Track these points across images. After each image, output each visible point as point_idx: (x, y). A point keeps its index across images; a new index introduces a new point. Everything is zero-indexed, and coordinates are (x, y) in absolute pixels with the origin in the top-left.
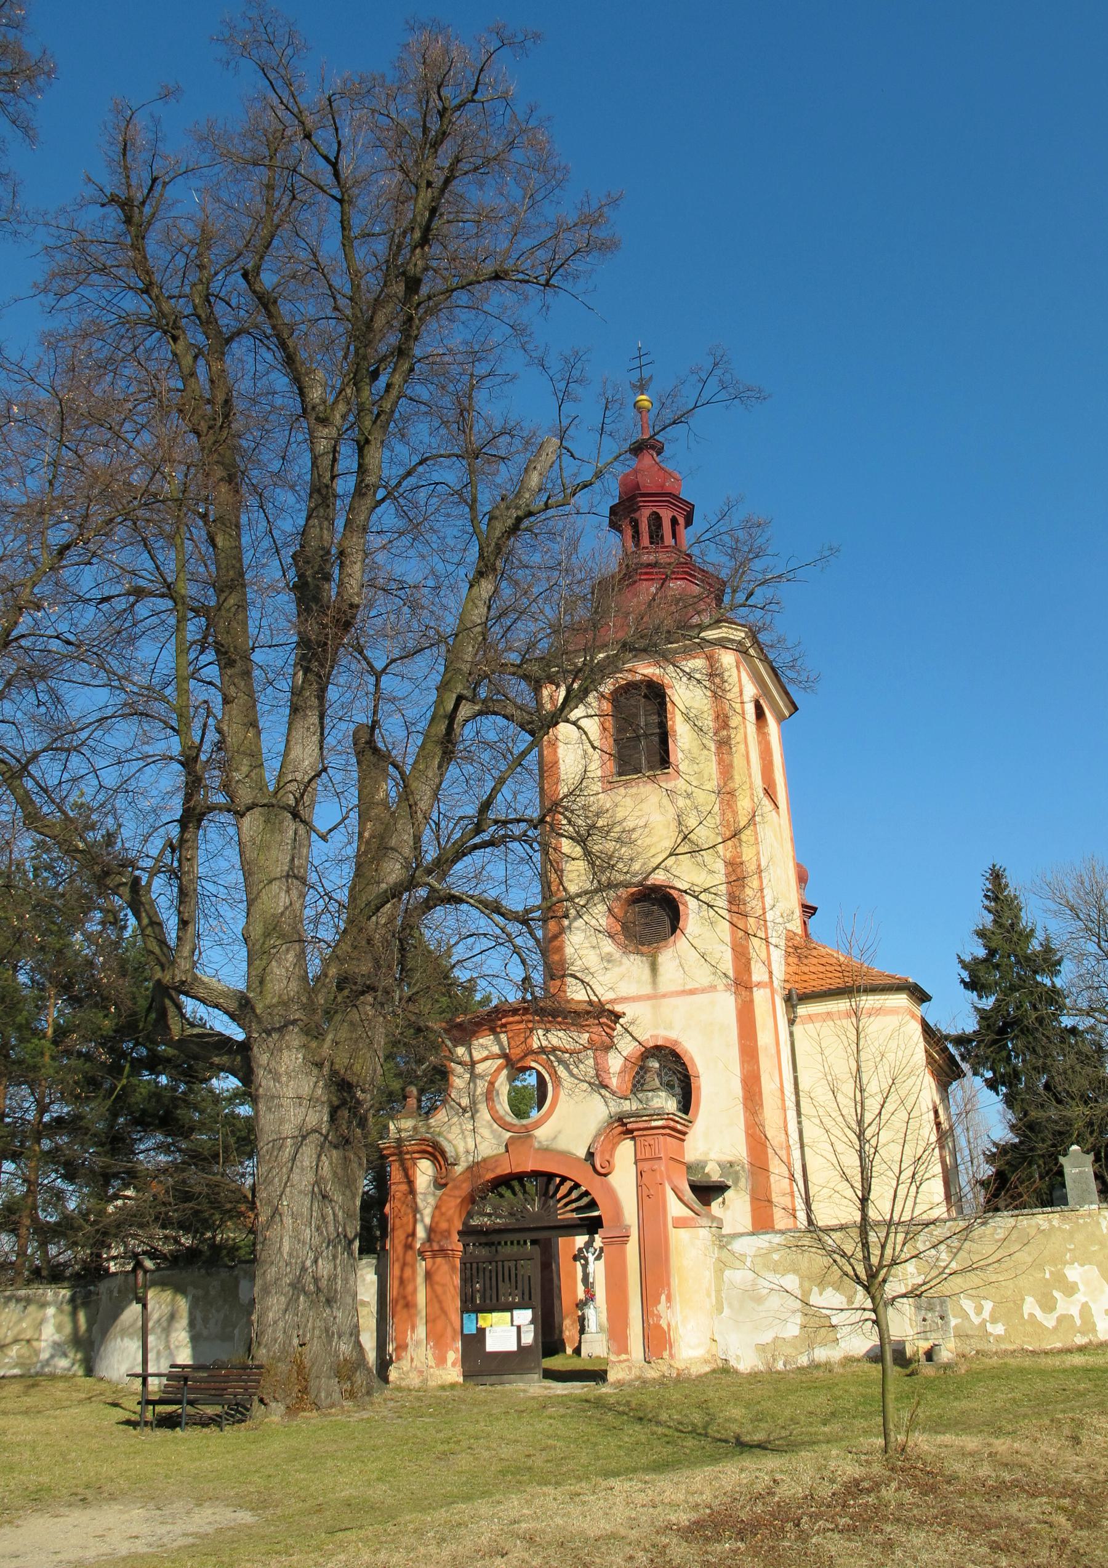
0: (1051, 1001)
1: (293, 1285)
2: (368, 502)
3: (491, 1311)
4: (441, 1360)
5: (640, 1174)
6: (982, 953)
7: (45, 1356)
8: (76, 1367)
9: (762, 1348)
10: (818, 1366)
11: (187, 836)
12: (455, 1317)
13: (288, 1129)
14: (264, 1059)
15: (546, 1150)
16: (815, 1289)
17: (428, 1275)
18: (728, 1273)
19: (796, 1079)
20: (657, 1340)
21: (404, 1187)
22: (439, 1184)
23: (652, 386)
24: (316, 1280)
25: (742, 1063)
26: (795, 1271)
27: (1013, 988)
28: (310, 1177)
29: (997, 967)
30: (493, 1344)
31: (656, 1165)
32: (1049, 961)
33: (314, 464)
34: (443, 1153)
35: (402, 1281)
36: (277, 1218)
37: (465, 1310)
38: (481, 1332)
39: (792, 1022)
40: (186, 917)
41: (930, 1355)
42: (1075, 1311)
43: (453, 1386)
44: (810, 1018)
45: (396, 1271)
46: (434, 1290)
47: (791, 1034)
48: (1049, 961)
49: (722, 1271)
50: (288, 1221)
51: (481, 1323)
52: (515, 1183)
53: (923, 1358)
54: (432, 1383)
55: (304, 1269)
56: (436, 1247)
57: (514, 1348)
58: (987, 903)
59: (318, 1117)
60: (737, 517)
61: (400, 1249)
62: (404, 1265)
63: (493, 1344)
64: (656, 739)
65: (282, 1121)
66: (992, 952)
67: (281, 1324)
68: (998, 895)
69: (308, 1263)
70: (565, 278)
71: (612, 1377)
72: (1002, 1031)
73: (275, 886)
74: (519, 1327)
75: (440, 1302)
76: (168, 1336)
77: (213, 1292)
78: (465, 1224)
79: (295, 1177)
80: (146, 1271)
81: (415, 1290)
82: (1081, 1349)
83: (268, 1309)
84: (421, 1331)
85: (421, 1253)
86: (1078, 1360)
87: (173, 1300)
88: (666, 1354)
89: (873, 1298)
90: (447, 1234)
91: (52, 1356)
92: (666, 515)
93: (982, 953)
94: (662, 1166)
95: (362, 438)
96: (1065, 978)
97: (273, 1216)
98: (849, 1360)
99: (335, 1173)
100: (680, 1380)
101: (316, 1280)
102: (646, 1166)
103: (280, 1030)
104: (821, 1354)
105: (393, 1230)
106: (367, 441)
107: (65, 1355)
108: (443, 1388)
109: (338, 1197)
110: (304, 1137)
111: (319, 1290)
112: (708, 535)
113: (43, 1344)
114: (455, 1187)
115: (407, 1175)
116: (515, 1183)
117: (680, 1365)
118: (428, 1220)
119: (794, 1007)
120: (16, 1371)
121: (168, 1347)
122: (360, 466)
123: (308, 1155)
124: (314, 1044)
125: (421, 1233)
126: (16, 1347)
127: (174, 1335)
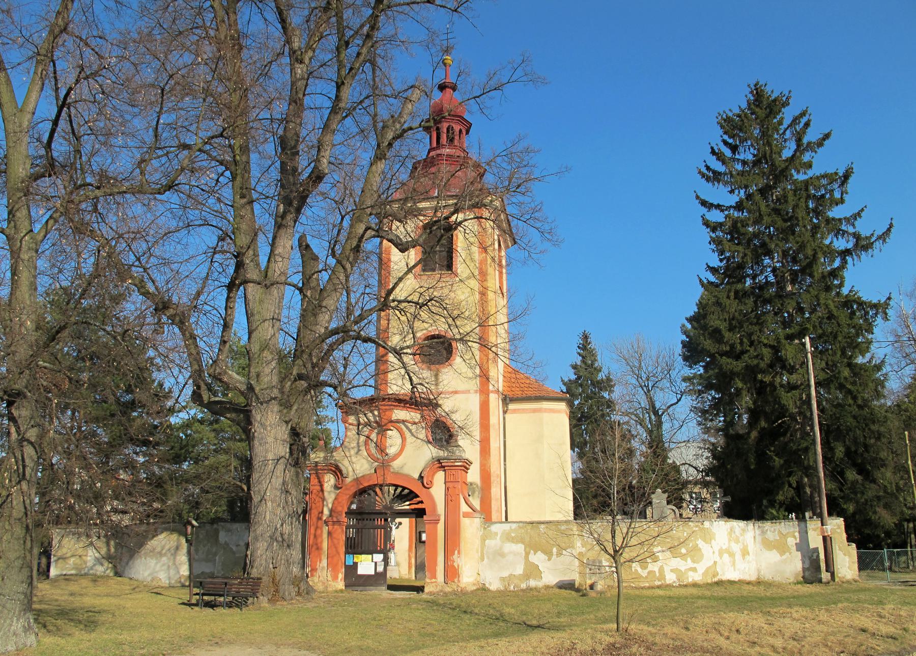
0: (609, 407)
1: (271, 537)
2: (339, 117)
3: (361, 554)
4: (335, 578)
5: (447, 489)
6: (573, 377)
7: (90, 564)
8: (109, 571)
9: (503, 579)
10: (531, 589)
11: (232, 295)
12: (342, 556)
13: (270, 456)
14: (258, 417)
15: (397, 474)
16: (532, 552)
17: (329, 533)
18: (487, 542)
19: (505, 442)
20: (451, 573)
21: (318, 488)
22: (336, 487)
23: (453, 52)
24: (282, 535)
25: (481, 432)
26: (523, 543)
27: (589, 397)
28: (281, 480)
29: (581, 385)
30: (361, 571)
31: (456, 485)
32: (608, 384)
33: (293, 84)
34: (341, 471)
35: (315, 536)
36: (263, 502)
37: (347, 552)
38: (356, 564)
39: (505, 412)
40: (226, 339)
41: (592, 587)
42: (656, 569)
43: (341, 591)
44: (515, 411)
45: (313, 531)
46: (332, 542)
47: (504, 418)
48: (608, 384)
49: (485, 540)
50: (269, 504)
51: (356, 560)
52: (378, 490)
53: (588, 589)
54: (330, 589)
55: (276, 529)
56: (335, 520)
57: (373, 573)
58: (579, 351)
59: (284, 450)
60: (520, 147)
61: (315, 519)
62: (317, 528)
63: (361, 571)
64: (445, 254)
65: (267, 451)
66: (579, 378)
67: (264, 557)
68: (585, 346)
69: (278, 526)
70: (466, 9)
71: (426, 590)
72: (579, 420)
73: (266, 323)
74: (376, 563)
75: (336, 548)
76: (175, 558)
77: (201, 536)
78: (349, 508)
79: (273, 480)
80: (193, 526)
81: (321, 542)
82: (659, 587)
83: (258, 549)
84: (324, 562)
85: (326, 522)
86: (660, 592)
87: (178, 539)
88: (456, 580)
89: (616, 562)
90: (340, 513)
91: (94, 565)
92: (457, 128)
93: (573, 377)
94: (459, 486)
95: (340, 81)
96: (617, 394)
97: (261, 501)
98: (547, 587)
99: (292, 480)
100: (464, 593)
101: (282, 535)
102: (450, 485)
103: (268, 402)
104: (533, 583)
105: (310, 509)
106: (343, 83)
107: (102, 565)
108: (336, 591)
109: (294, 492)
110: (278, 460)
111: (283, 540)
112: (504, 153)
113: (89, 558)
114: (346, 489)
115: (320, 482)
116: (378, 490)
117: (462, 585)
118: (330, 506)
119: (507, 404)
120: (73, 572)
121: (174, 564)
122: (337, 96)
123: (281, 467)
124: (285, 411)
125: (326, 512)
126: (72, 560)
127: (178, 558)
